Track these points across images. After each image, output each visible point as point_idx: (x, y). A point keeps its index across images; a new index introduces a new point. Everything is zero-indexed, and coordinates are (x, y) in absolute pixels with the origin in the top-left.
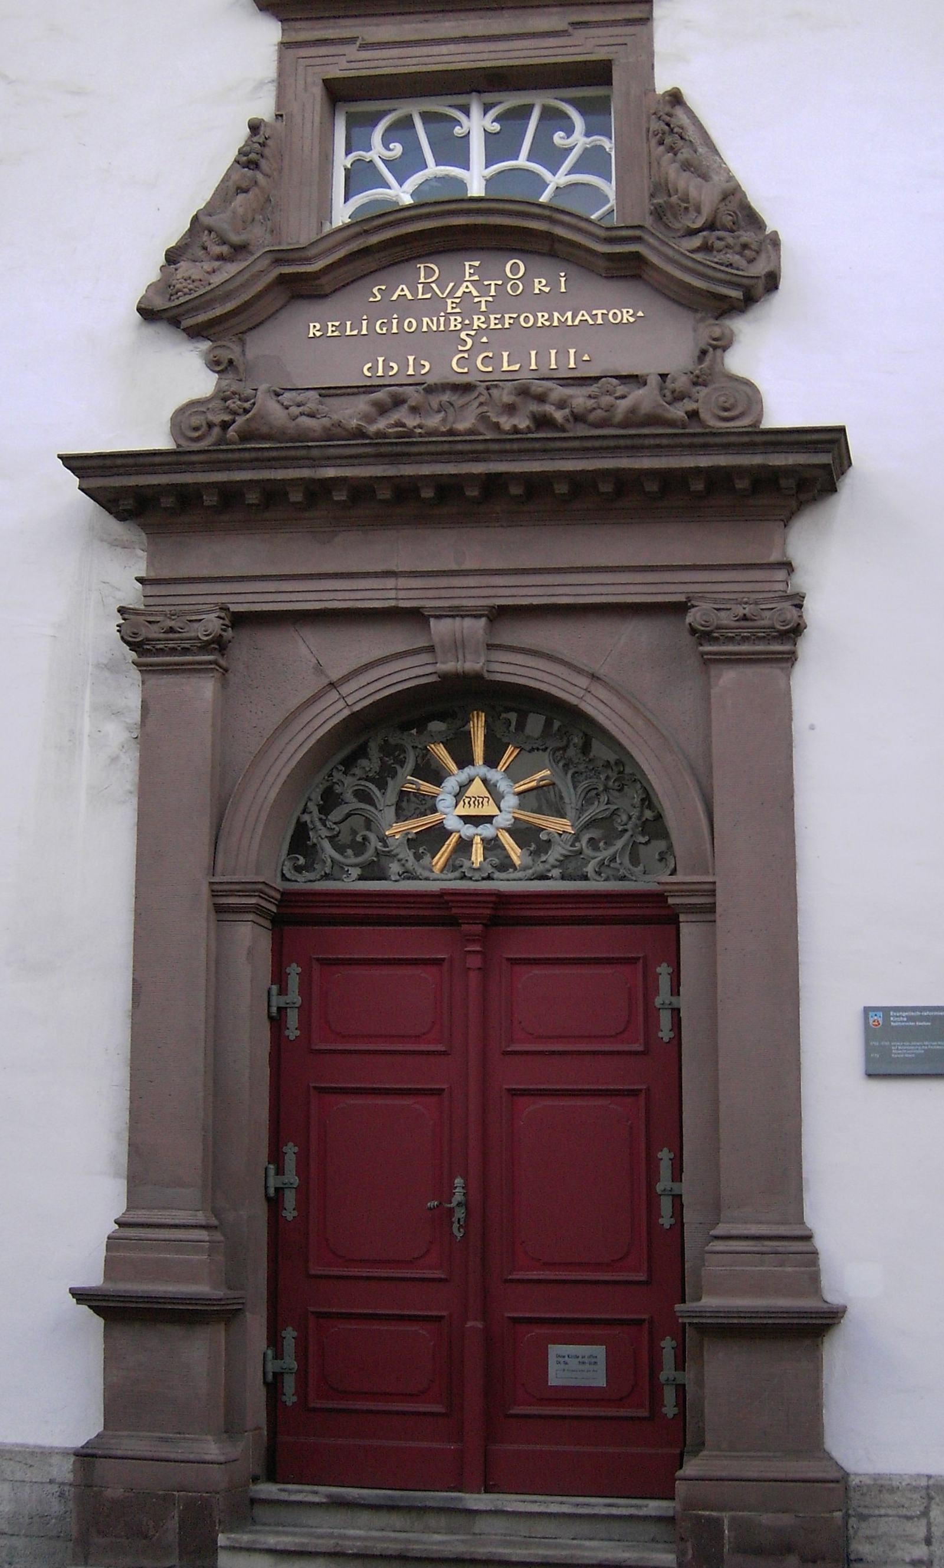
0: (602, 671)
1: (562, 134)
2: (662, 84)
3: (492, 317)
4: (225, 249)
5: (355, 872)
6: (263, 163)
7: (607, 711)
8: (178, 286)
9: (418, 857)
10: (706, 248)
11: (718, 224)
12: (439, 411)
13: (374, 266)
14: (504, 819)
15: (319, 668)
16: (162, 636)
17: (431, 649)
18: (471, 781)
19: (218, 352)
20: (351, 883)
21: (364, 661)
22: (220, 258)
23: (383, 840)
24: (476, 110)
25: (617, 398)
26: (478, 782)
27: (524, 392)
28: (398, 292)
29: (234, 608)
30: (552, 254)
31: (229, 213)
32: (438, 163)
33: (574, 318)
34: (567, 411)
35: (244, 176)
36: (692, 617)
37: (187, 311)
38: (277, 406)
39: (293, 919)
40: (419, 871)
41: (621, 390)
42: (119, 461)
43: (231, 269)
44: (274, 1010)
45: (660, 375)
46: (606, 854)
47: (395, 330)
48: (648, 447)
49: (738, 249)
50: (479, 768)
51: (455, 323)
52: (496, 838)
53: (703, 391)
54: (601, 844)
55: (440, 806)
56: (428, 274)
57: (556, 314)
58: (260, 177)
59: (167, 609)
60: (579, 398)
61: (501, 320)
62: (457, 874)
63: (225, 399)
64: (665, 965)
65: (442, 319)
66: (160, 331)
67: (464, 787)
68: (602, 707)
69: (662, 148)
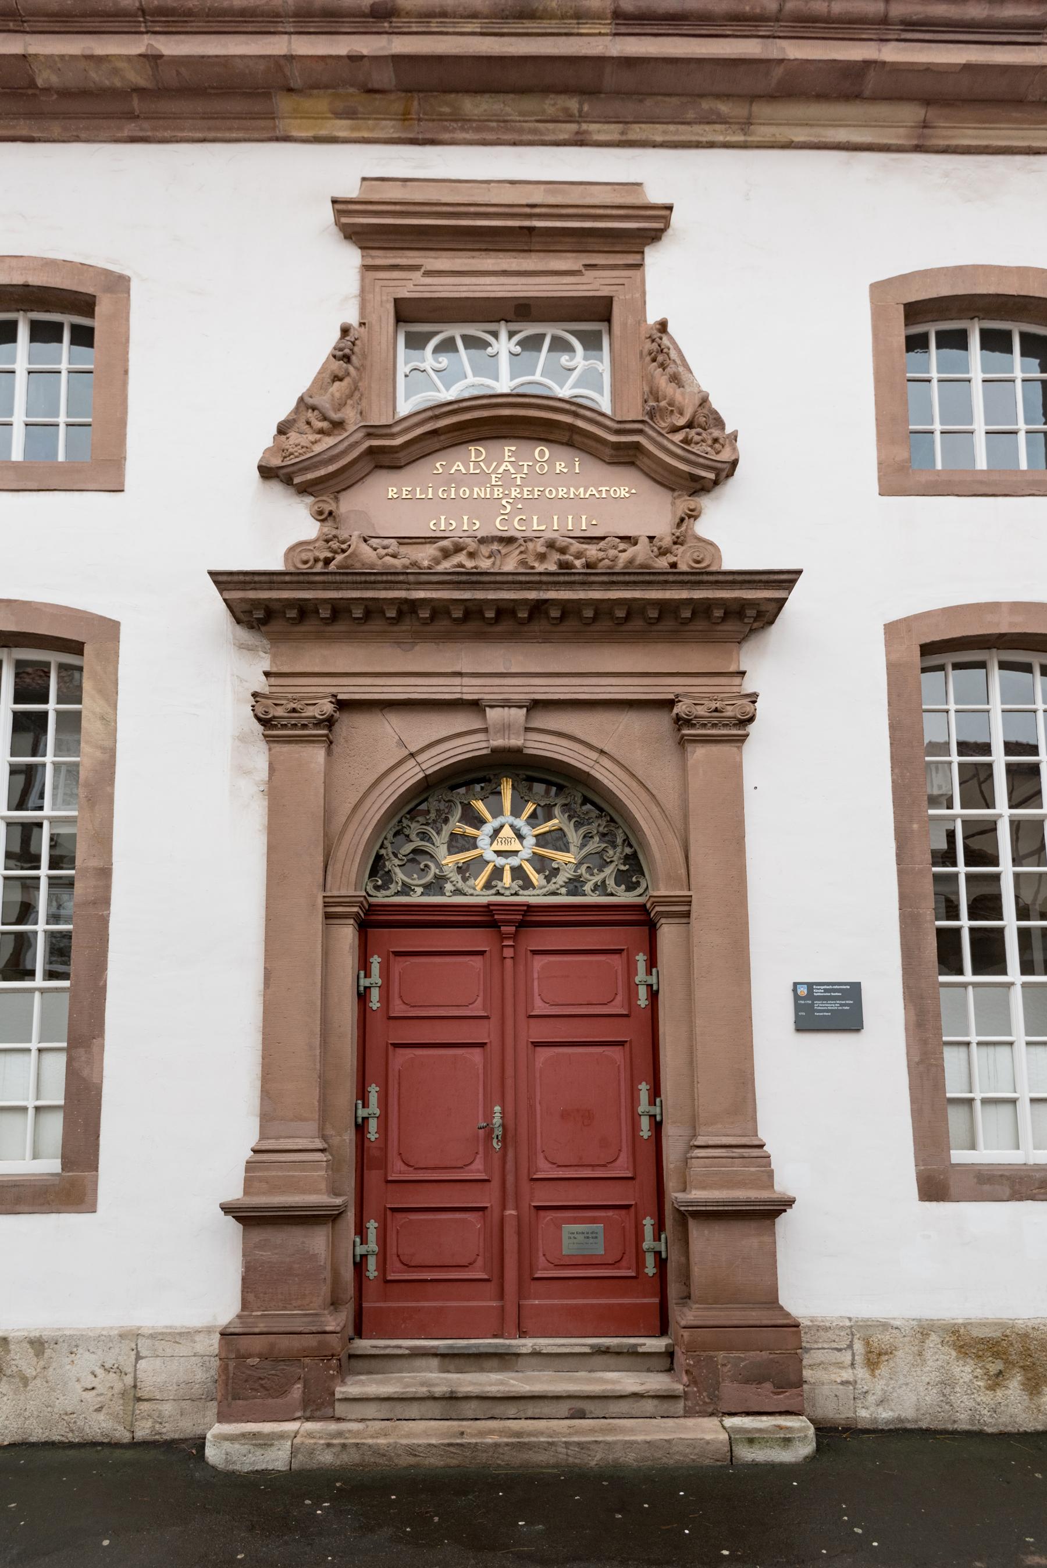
0: (606, 749)
1: (567, 357)
2: (652, 318)
3: (525, 489)
4: (325, 425)
5: (419, 890)
6: (354, 358)
7: (610, 776)
8: (291, 450)
9: (465, 879)
10: (686, 441)
11: (696, 424)
12: (489, 557)
13: (438, 446)
14: (526, 853)
15: (402, 743)
16: (286, 715)
17: (485, 730)
18: (502, 827)
19: (321, 505)
20: (417, 898)
21: (434, 739)
22: (321, 432)
23: (439, 866)
24: (503, 335)
25: (621, 551)
26: (507, 828)
27: (551, 545)
28: (455, 468)
29: (340, 697)
30: (570, 444)
31: (328, 396)
32: (474, 376)
33: (585, 492)
34: (584, 560)
35: (340, 368)
36: (680, 709)
37: (300, 470)
38: (367, 548)
39: (371, 922)
40: (466, 890)
41: (622, 546)
42: (256, 578)
43: (329, 442)
44: (362, 989)
45: (649, 537)
46: (598, 878)
47: (453, 496)
48: (659, 582)
49: (710, 442)
50: (507, 818)
51: (497, 493)
52: (520, 867)
53: (680, 550)
54: (595, 871)
55: (480, 843)
56: (475, 457)
57: (572, 489)
58: (351, 369)
59: (290, 696)
60: (592, 551)
61: (531, 492)
62: (493, 891)
63: (327, 541)
64: (641, 954)
65: (488, 490)
66: (276, 488)
67: (497, 832)
68: (607, 773)
69: (655, 364)
